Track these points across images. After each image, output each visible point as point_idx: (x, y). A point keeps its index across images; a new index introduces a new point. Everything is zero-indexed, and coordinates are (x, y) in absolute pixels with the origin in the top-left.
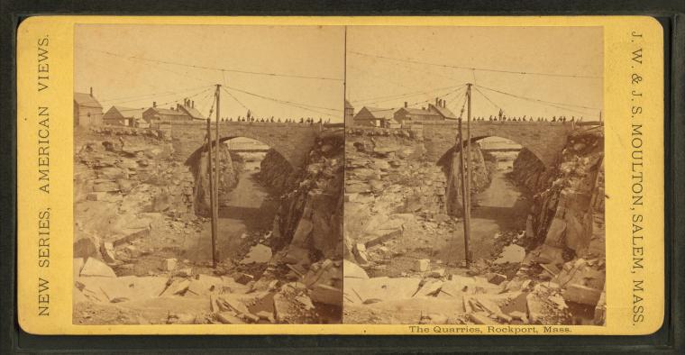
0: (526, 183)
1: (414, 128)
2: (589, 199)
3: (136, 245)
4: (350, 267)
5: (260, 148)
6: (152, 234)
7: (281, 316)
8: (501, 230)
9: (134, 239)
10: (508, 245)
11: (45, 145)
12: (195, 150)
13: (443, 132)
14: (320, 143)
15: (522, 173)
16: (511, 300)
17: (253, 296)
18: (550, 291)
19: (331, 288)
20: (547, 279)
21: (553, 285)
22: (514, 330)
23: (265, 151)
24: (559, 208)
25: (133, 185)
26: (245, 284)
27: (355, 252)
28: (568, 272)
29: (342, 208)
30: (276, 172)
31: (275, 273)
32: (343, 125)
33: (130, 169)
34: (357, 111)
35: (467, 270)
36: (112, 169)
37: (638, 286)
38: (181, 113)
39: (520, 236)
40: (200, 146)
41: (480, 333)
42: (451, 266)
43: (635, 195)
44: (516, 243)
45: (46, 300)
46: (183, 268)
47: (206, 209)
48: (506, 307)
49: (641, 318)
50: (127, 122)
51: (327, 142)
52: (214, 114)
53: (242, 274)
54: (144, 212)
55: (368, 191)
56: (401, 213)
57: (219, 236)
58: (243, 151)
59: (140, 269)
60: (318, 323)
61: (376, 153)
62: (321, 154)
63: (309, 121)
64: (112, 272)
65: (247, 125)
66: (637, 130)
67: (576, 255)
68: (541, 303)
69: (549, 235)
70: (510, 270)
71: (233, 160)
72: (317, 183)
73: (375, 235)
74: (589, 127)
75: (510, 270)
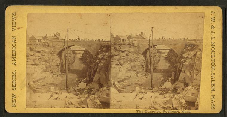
0: (172, 61)
1: (134, 42)
2: (193, 66)
3: (125, 82)
4: (112, 90)
5: (167, 48)
6: (46, 79)
7: (89, 106)
8: (78, 77)
9: (125, 80)
10: (80, 82)
11: (14, 49)
12: (145, 50)
13: (59, 44)
14: (102, 48)
15: (85, 58)
16: (81, 101)
17: (80, 100)
18: (95, 98)
19: (191, 96)
20: (94, 94)
21: (96, 96)
22: (172, 112)
23: (169, 49)
24: (98, 70)
25: (124, 62)
26: (162, 95)
27: (114, 84)
28: (101, 92)
29: (110, 69)
30: (87, 58)
31: (87, 92)
32: (110, 41)
33: (123, 57)
34: (115, 36)
35: (67, 91)
36: (117, 57)
37: (213, 97)
38: (56, 37)
39: (170, 79)
40: (62, 49)
41: (160, 113)
42: (147, 89)
43: (212, 66)
44: (168, 81)
45: (15, 101)
46: (56, 90)
47: (149, 70)
48: (165, 103)
49: (214, 108)
50: (37, 41)
51: (105, 47)
52: (67, 38)
53: (76, 92)
54: (128, 71)
55: (118, 64)
56: (45, 71)
57: (68, 79)
58: (76, 50)
59: (43, 91)
60: (102, 108)
61: (37, 51)
62: (102, 51)
63: (98, 40)
64: (117, 92)
65: (78, 42)
66: (213, 44)
67: (189, 85)
68: (92, 102)
69: (179, 78)
70: (166, 90)
71: (73, 53)
72: (186, 60)
73: (121, 79)
74: (193, 41)
75: (166, 90)
